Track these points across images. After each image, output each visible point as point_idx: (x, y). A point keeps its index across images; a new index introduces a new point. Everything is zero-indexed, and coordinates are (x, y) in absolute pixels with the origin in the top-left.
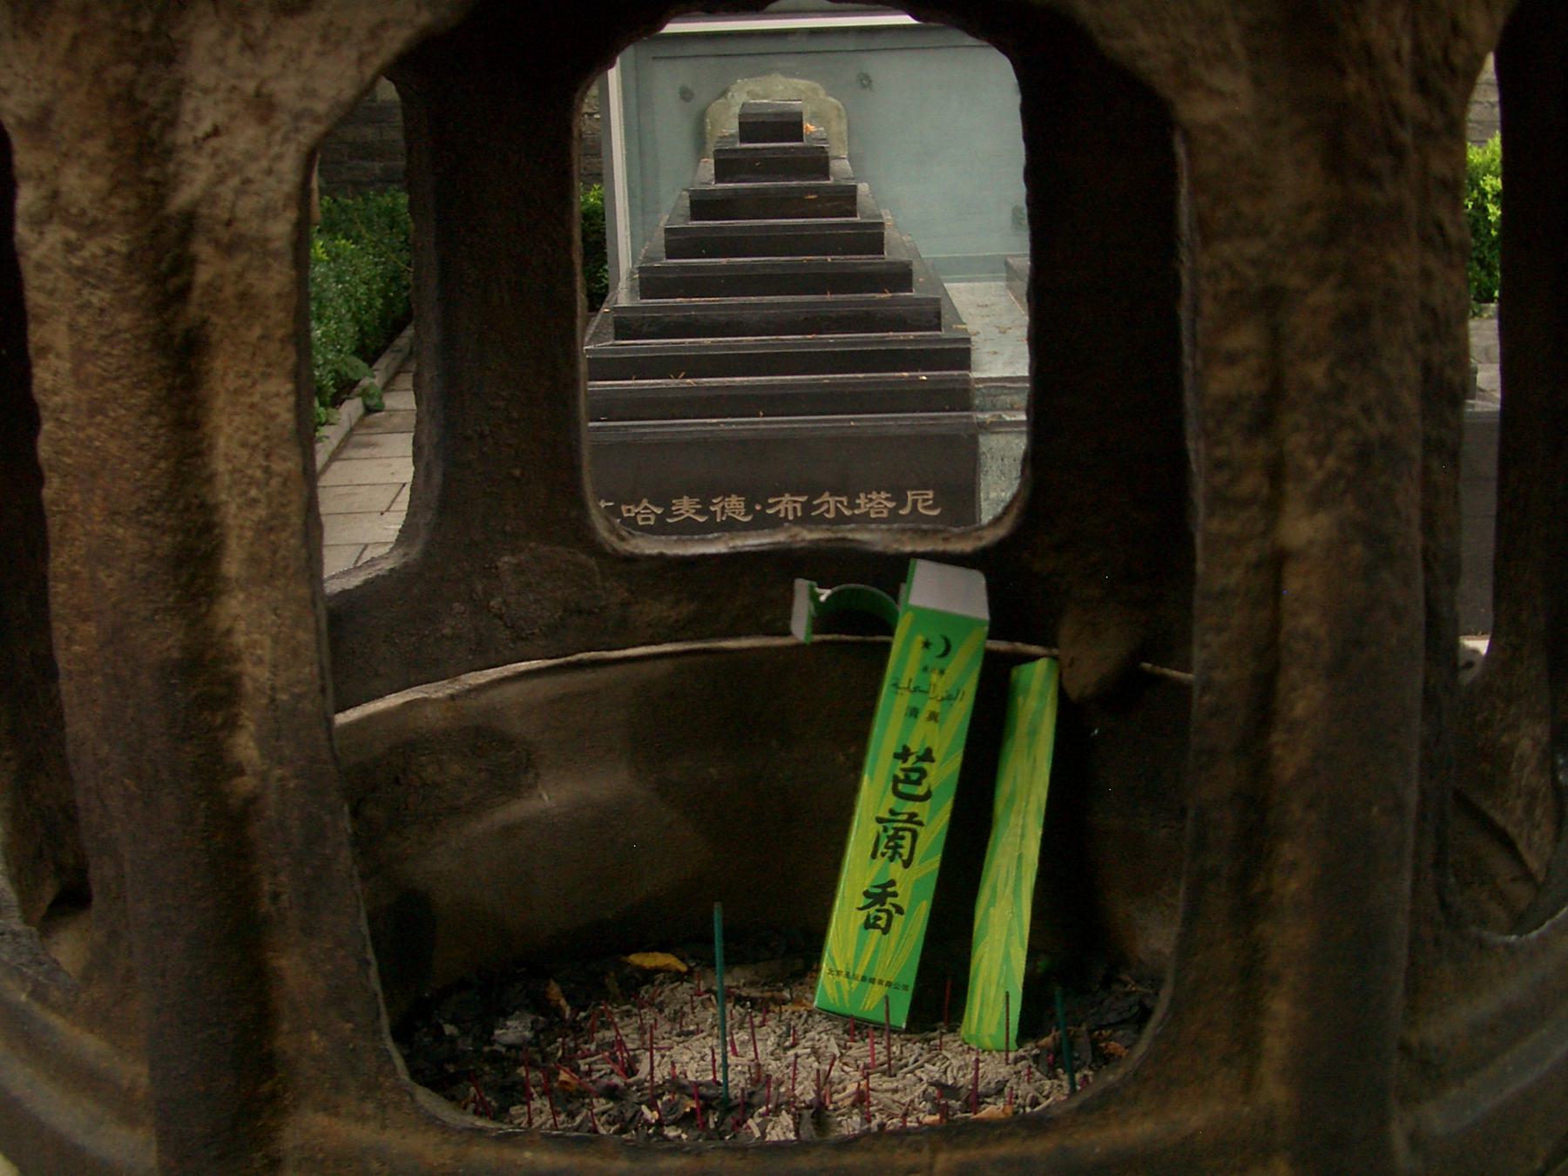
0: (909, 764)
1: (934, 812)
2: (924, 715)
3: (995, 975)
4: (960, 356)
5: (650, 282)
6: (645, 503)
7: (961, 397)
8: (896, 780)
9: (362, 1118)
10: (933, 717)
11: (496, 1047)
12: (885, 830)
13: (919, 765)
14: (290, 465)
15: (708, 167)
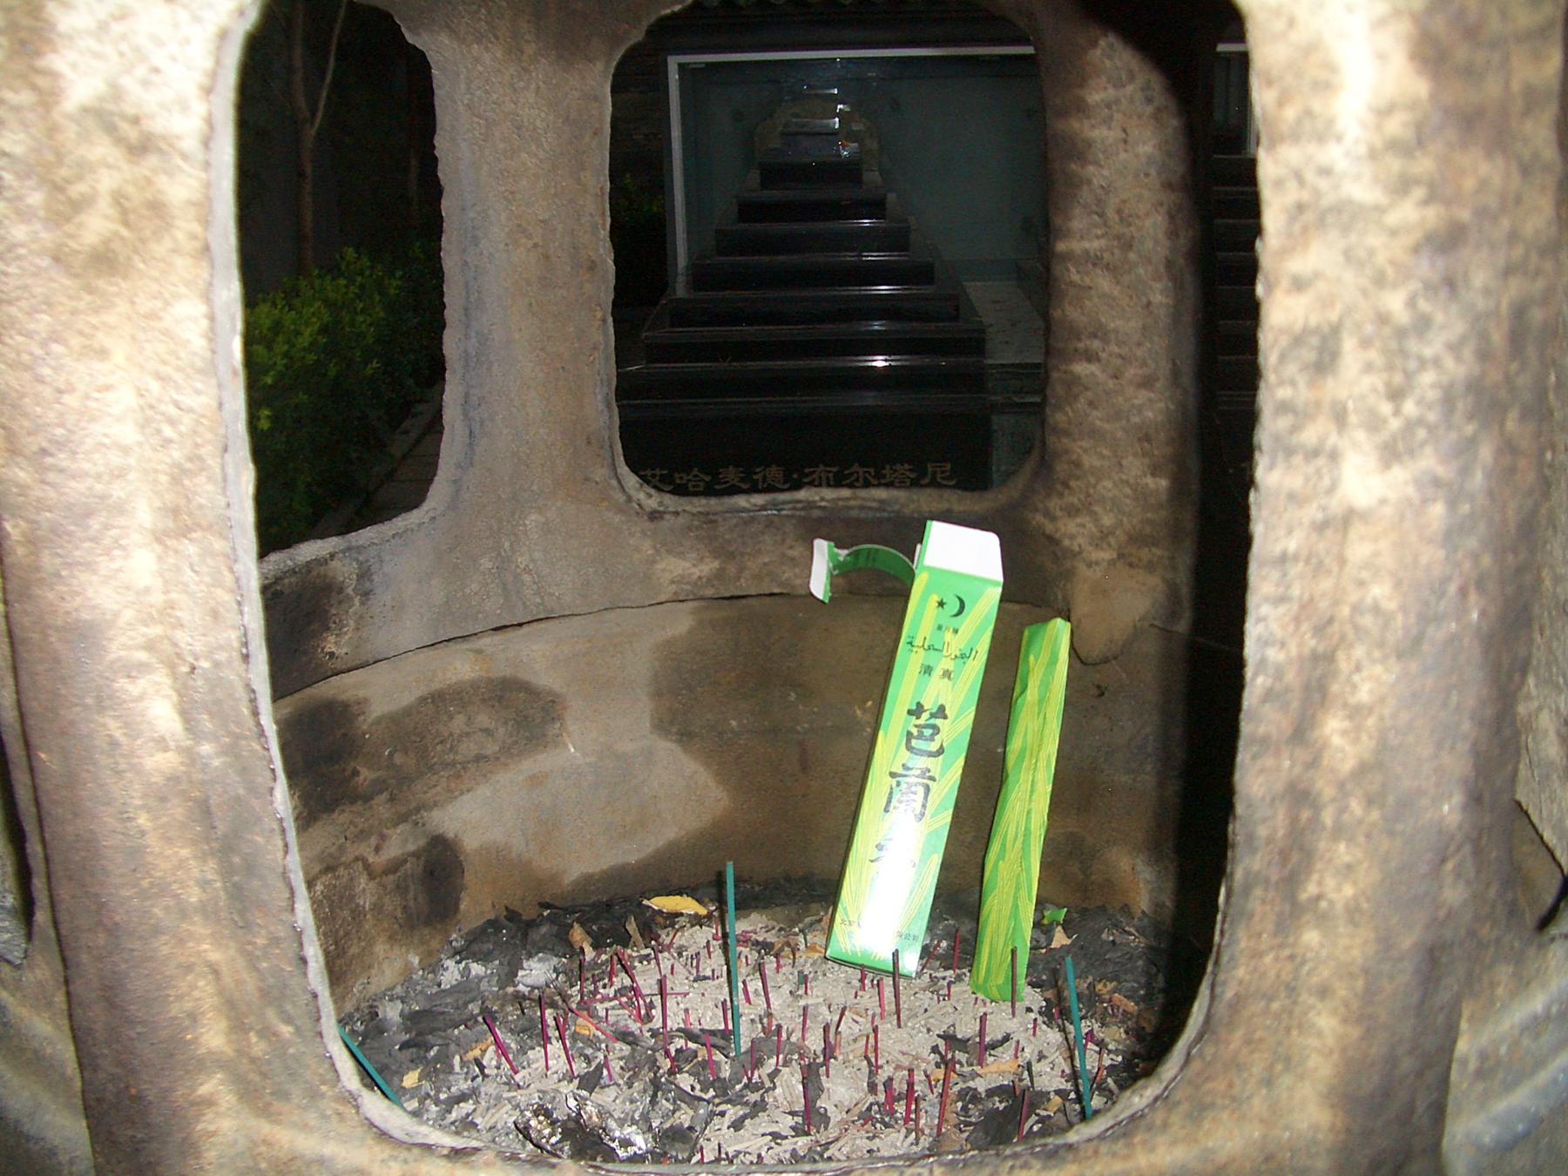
0: (921, 721)
1: (946, 768)
2: (938, 672)
3: (1003, 927)
4: (976, 344)
5: (701, 277)
6: (695, 471)
7: (975, 380)
8: (909, 735)
9: (305, 1127)
10: (947, 674)
11: (521, 987)
12: (898, 784)
13: (932, 721)
14: (204, 400)
15: (755, 177)
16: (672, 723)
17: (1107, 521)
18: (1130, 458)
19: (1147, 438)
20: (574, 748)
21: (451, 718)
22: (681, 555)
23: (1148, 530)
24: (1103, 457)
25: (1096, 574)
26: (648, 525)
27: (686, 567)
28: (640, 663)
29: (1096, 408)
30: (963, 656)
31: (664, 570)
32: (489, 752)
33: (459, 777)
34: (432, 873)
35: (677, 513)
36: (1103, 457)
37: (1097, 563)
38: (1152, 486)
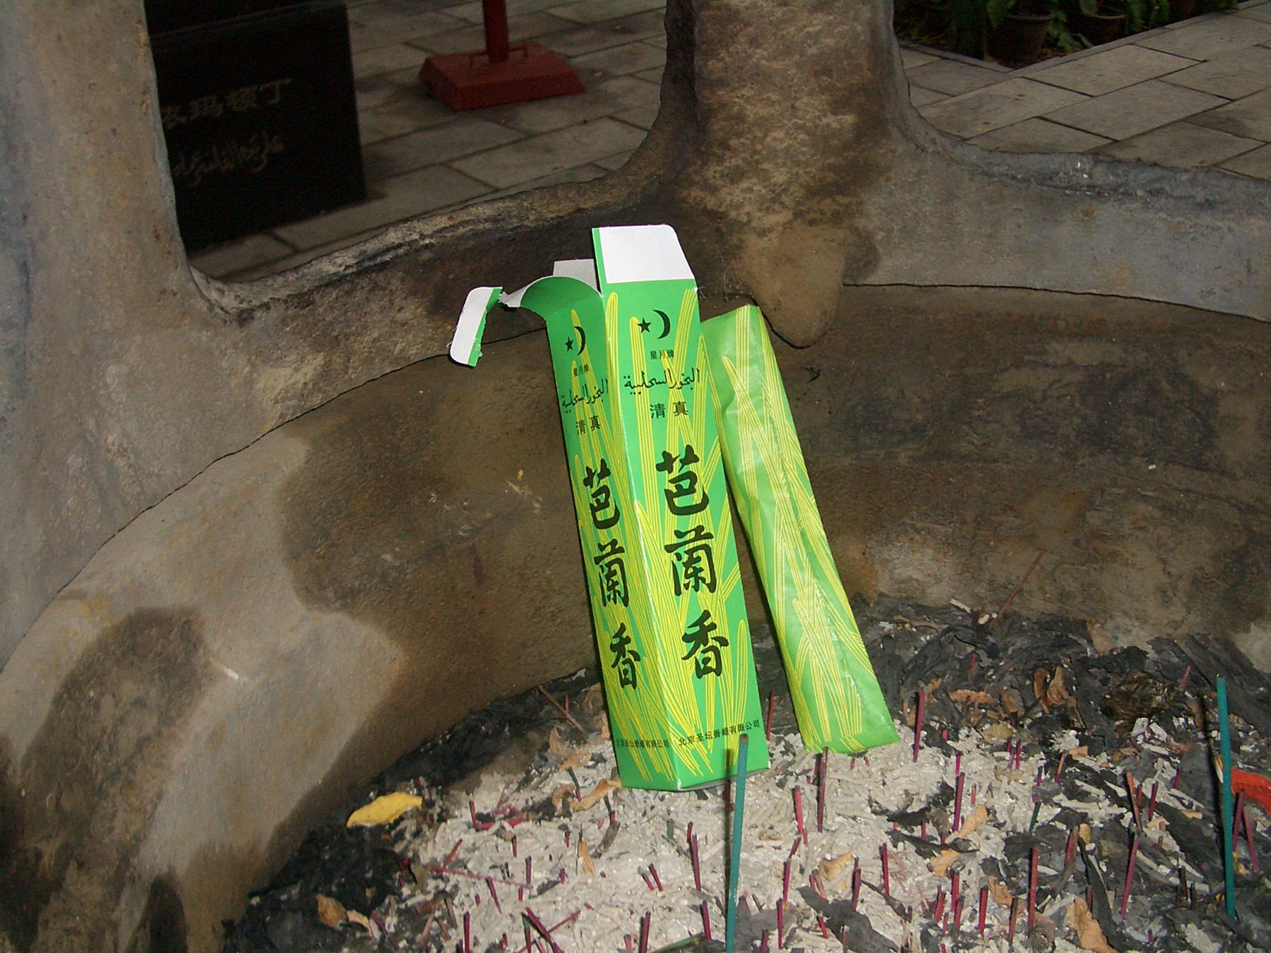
2: (670, 410)
16: (322, 588)
17: (779, 177)
18: (805, 99)
19: (827, 71)
20: (233, 674)
21: (97, 707)
22: (278, 362)
23: (831, 177)
24: (773, 103)
25: (773, 241)
26: (236, 334)
27: (288, 376)
28: (266, 526)
29: (759, 46)
30: (688, 381)
31: (264, 390)
32: (148, 730)
33: (130, 783)
34: (159, 934)
35: (266, 306)
36: (773, 103)
37: (770, 230)
38: (835, 125)
